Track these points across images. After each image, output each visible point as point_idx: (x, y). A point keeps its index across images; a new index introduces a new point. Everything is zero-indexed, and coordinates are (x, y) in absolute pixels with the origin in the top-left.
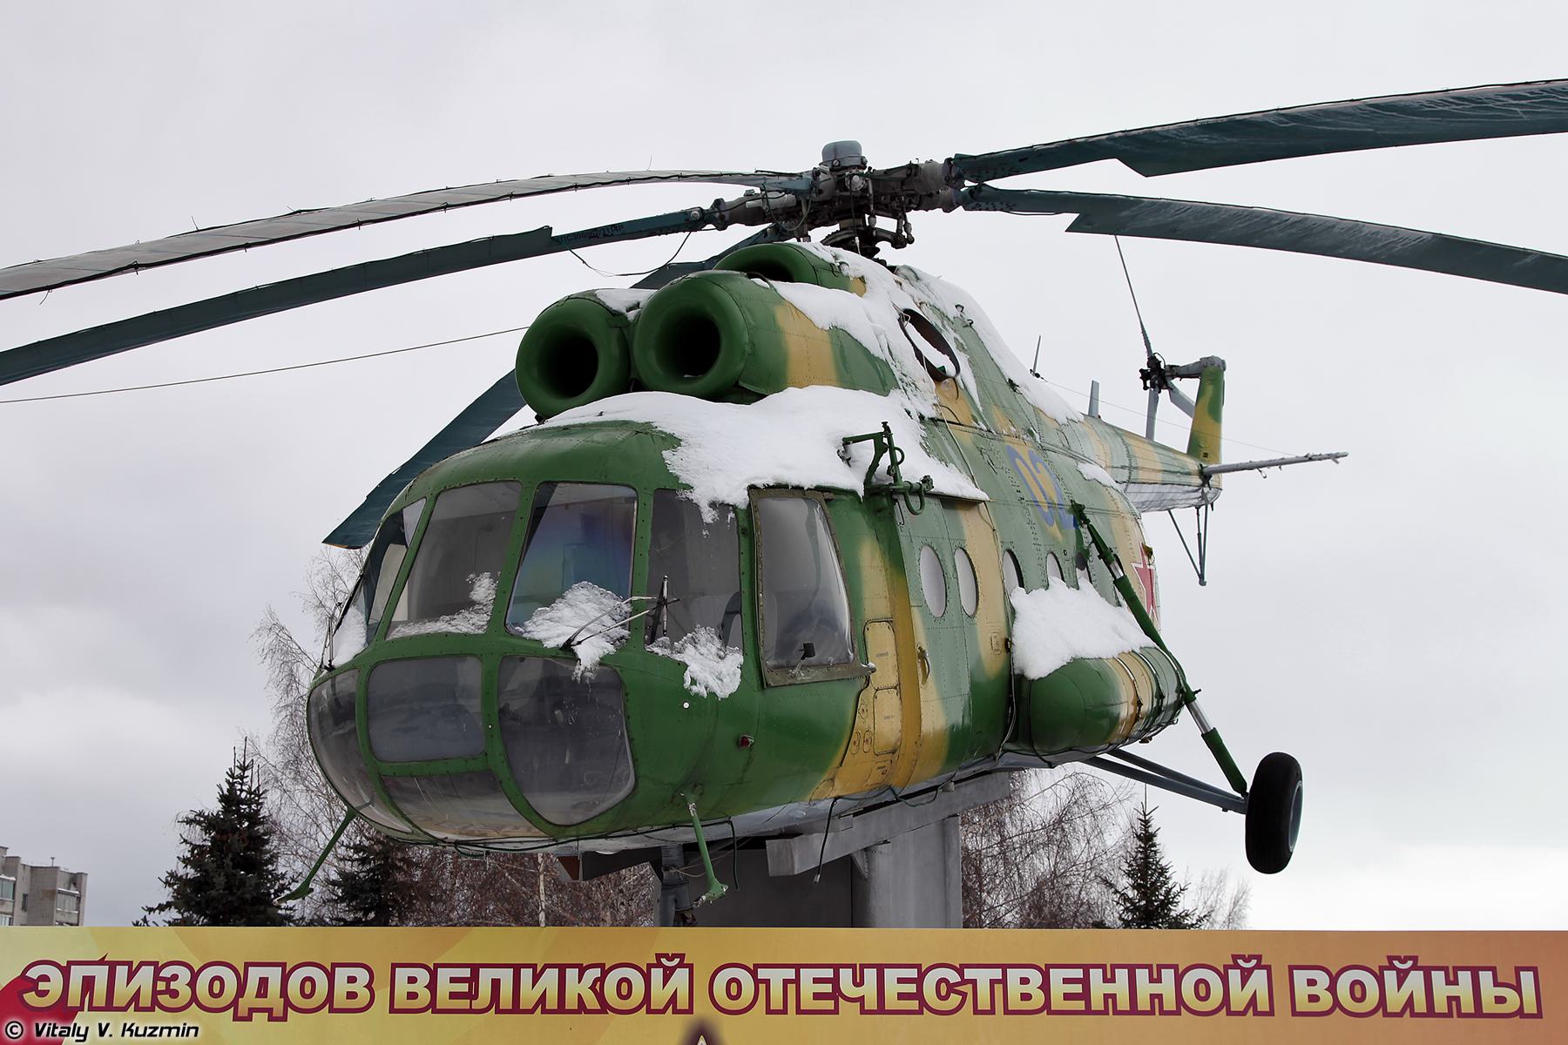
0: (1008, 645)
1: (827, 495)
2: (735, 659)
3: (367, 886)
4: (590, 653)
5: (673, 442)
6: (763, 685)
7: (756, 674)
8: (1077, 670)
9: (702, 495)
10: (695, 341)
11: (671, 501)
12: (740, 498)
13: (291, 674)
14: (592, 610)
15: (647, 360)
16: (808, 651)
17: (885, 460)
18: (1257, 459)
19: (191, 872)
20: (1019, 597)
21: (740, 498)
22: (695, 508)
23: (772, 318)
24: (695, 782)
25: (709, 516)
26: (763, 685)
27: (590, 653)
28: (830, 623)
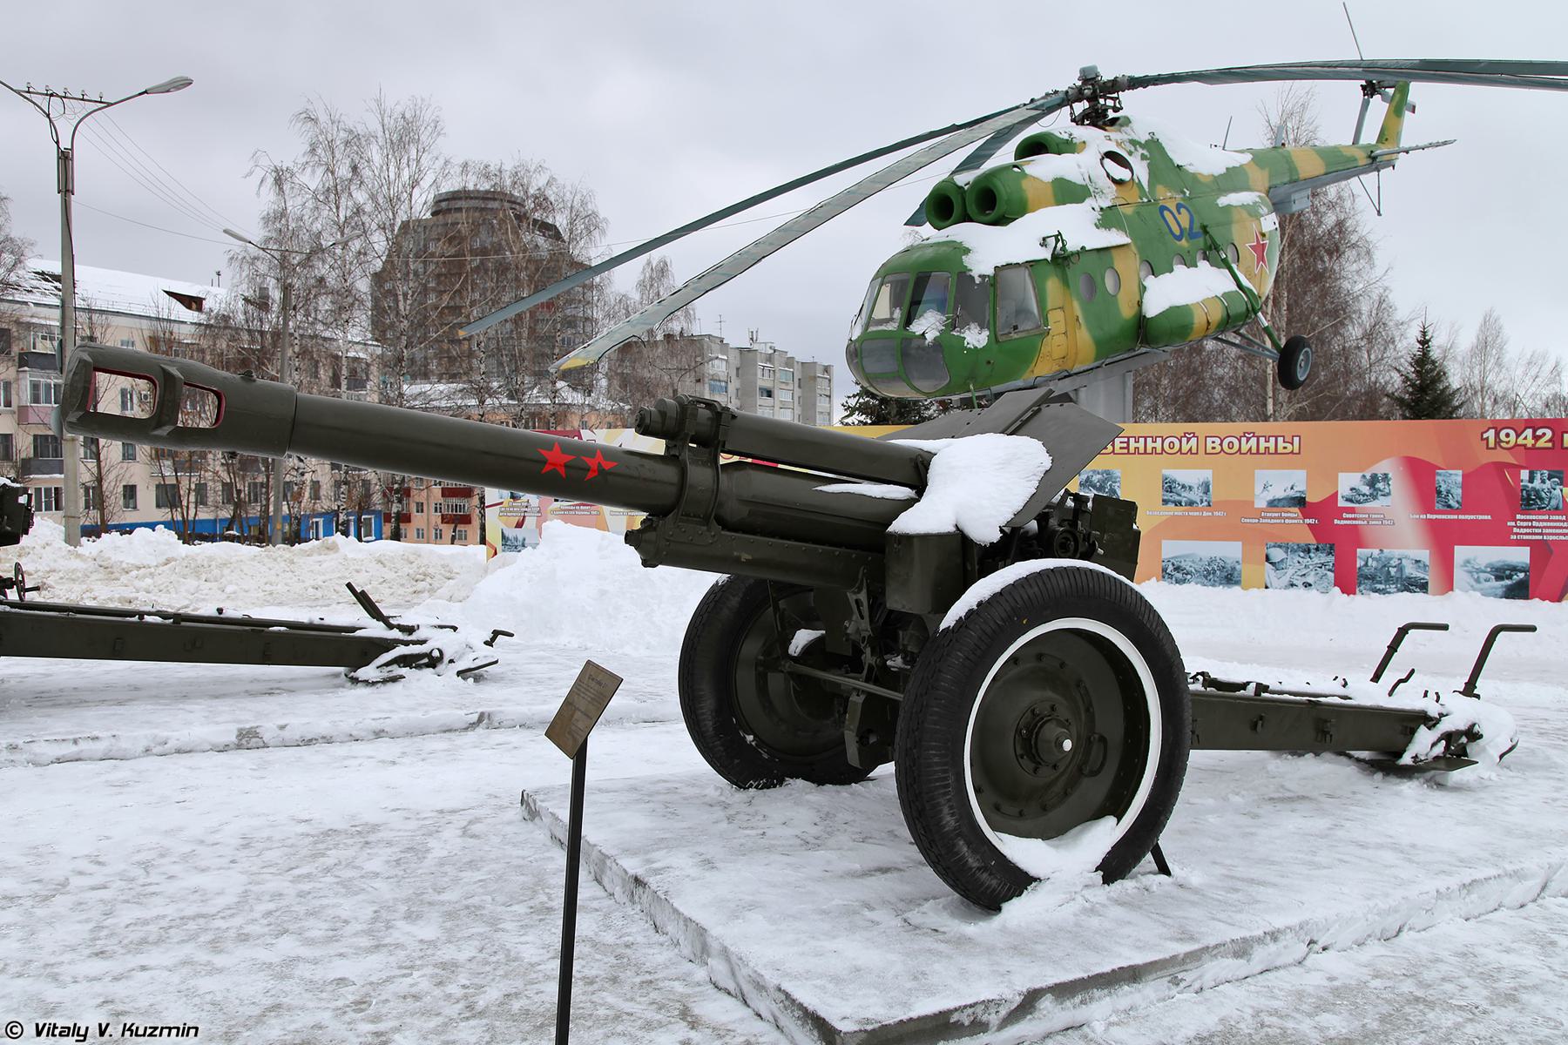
0: (1140, 304)
1: (1031, 264)
2: (986, 333)
3: (1098, 400)
4: (930, 337)
5: (967, 251)
6: (997, 341)
7: (994, 339)
8: (1173, 311)
9: (975, 274)
10: (989, 202)
11: (964, 276)
12: (991, 272)
13: (140, 943)
14: (932, 320)
15: (972, 209)
16: (1015, 328)
17: (1060, 245)
18: (1421, 144)
19: (1336, 347)
20: (1150, 282)
21: (991, 272)
22: (972, 278)
23: (1021, 190)
24: (972, 377)
25: (978, 280)
26: (997, 341)
27: (930, 337)
28: (1028, 312)
